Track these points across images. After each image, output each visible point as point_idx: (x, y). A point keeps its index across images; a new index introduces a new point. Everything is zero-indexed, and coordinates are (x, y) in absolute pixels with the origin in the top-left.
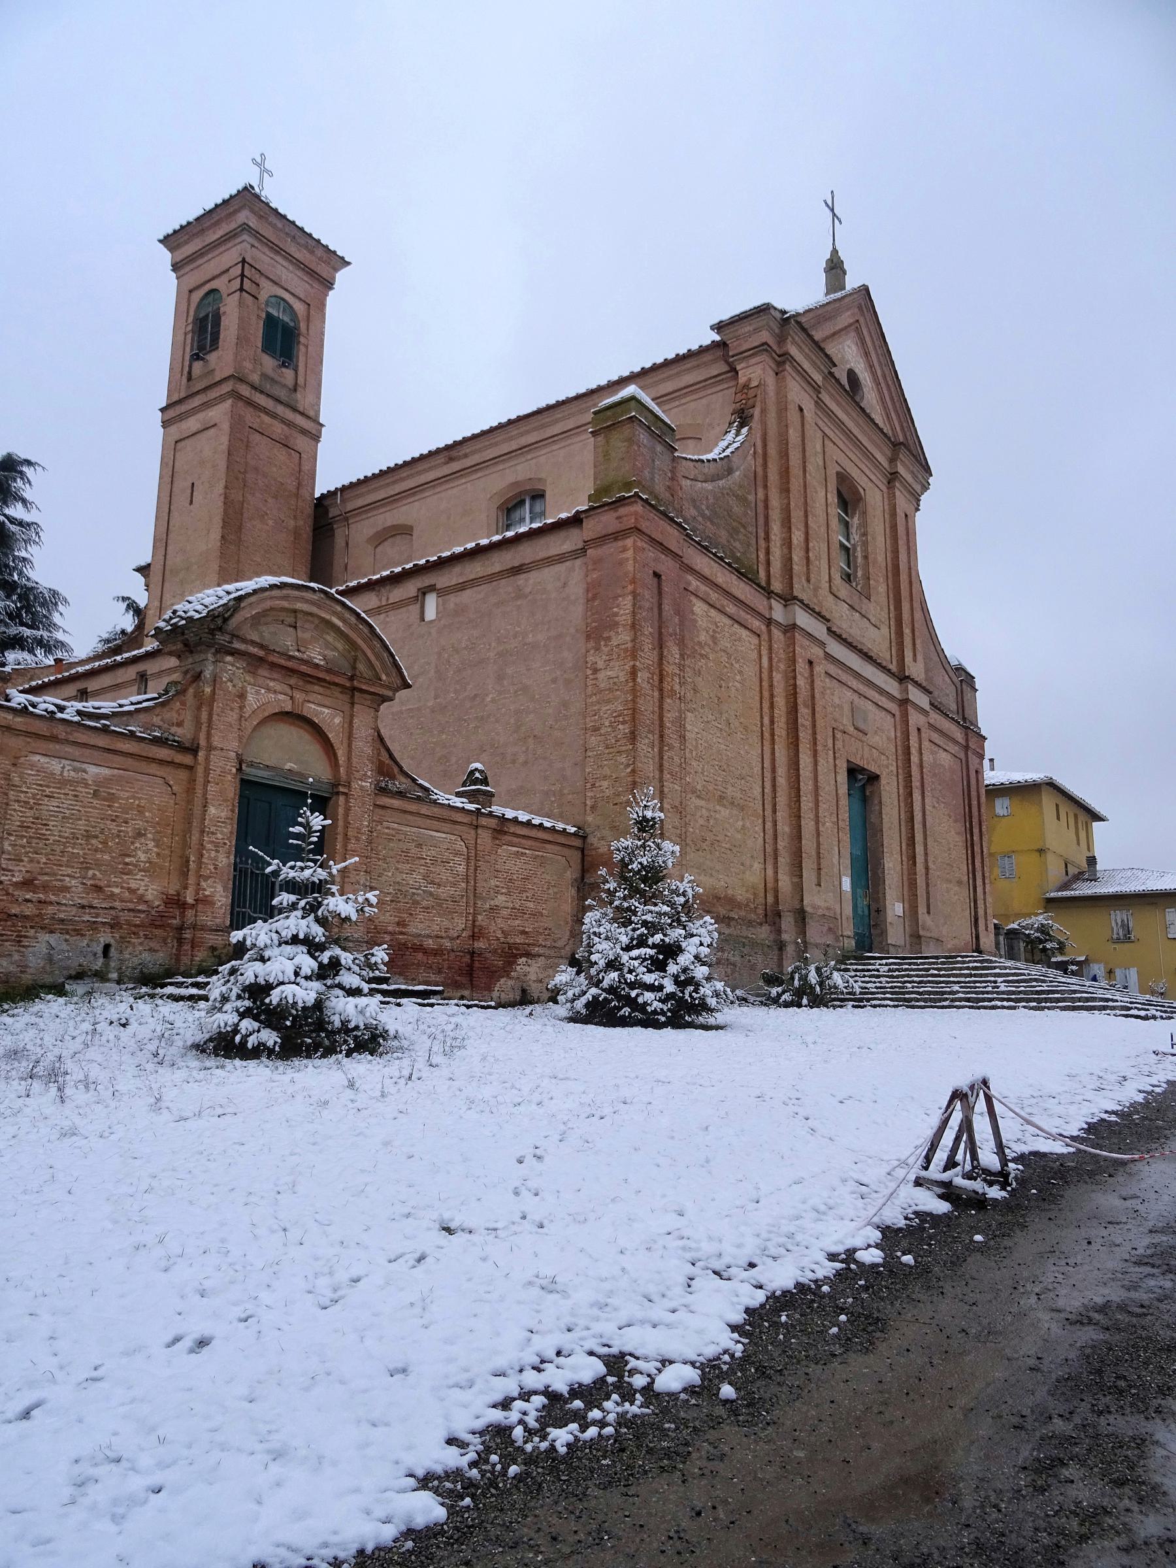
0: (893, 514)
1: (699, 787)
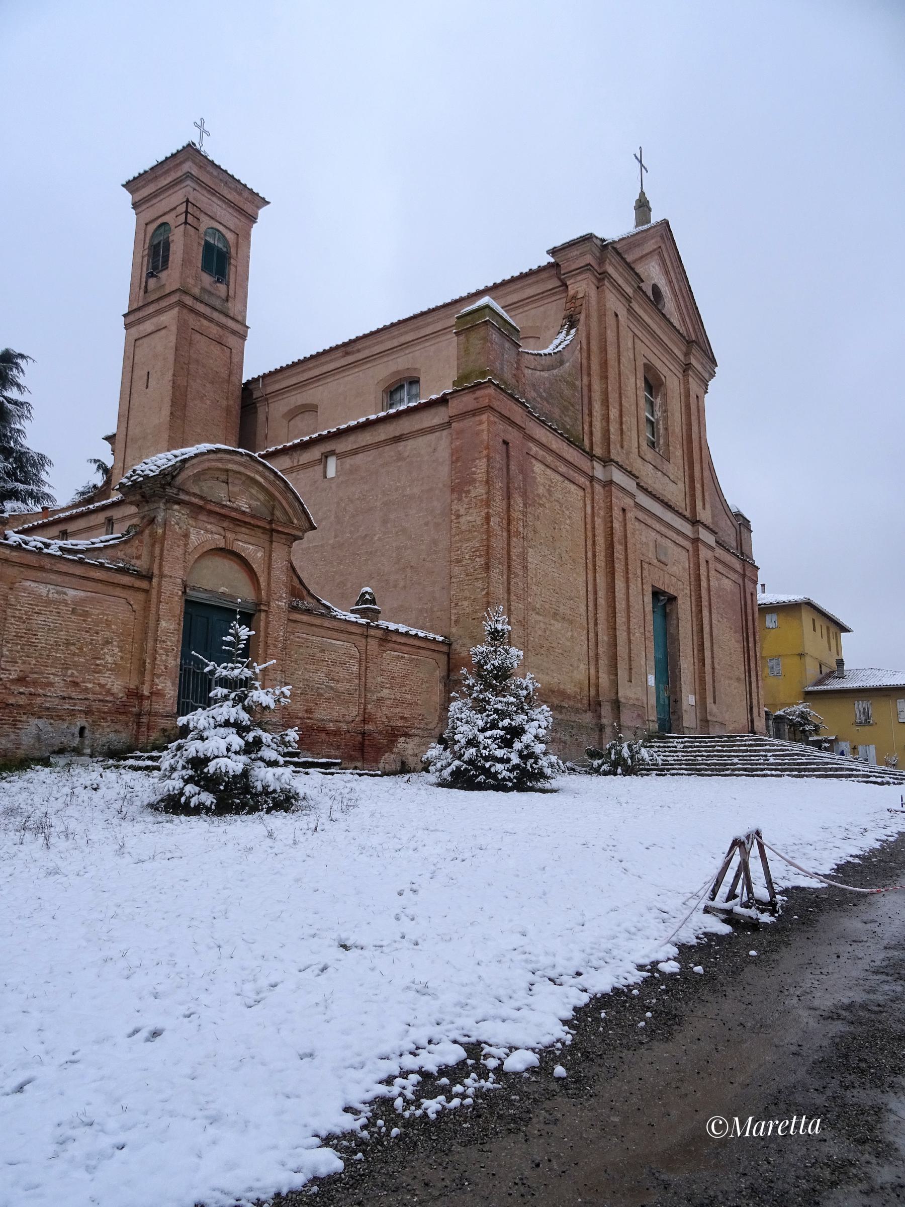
0: (688, 396)
1: (538, 606)
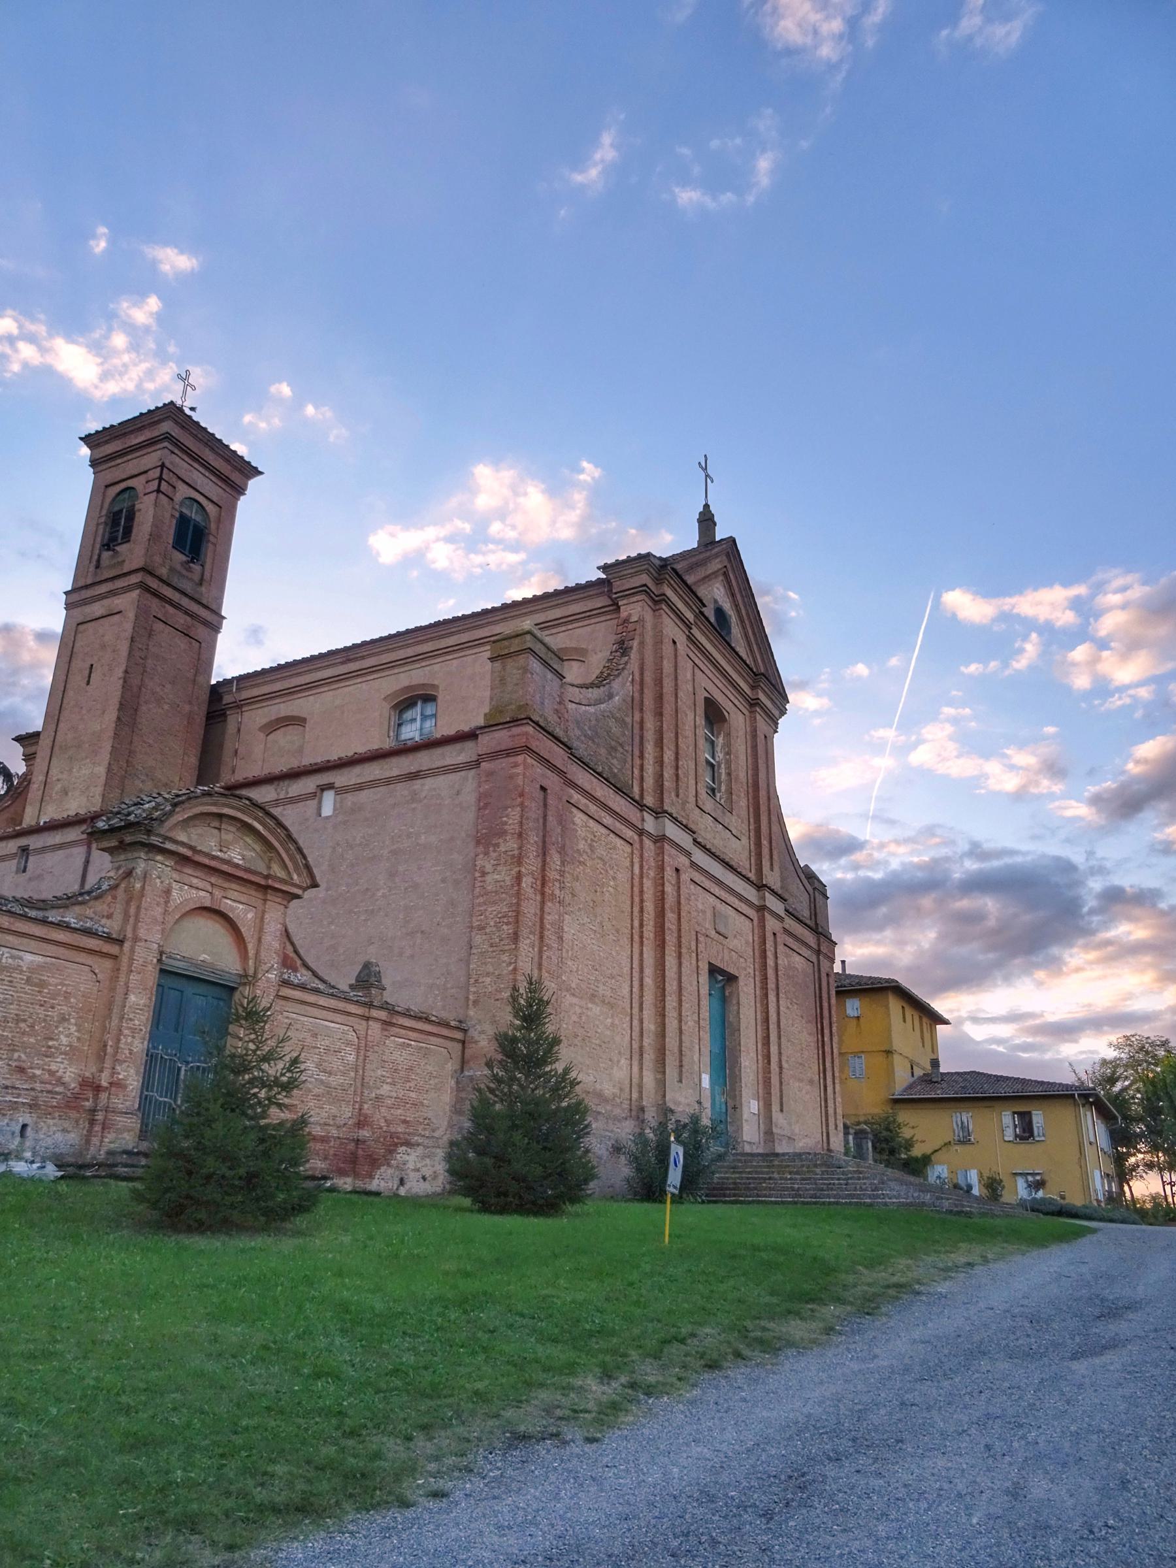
0: (754, 736)
1: (573, 985)
